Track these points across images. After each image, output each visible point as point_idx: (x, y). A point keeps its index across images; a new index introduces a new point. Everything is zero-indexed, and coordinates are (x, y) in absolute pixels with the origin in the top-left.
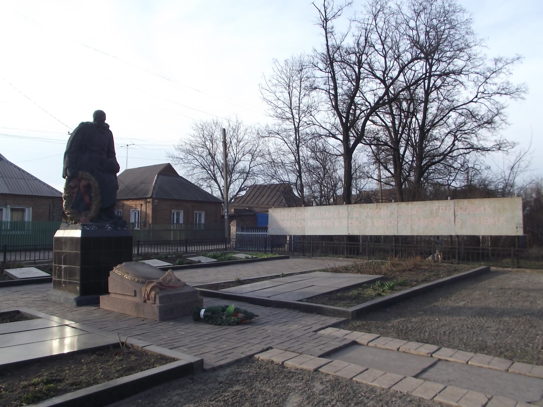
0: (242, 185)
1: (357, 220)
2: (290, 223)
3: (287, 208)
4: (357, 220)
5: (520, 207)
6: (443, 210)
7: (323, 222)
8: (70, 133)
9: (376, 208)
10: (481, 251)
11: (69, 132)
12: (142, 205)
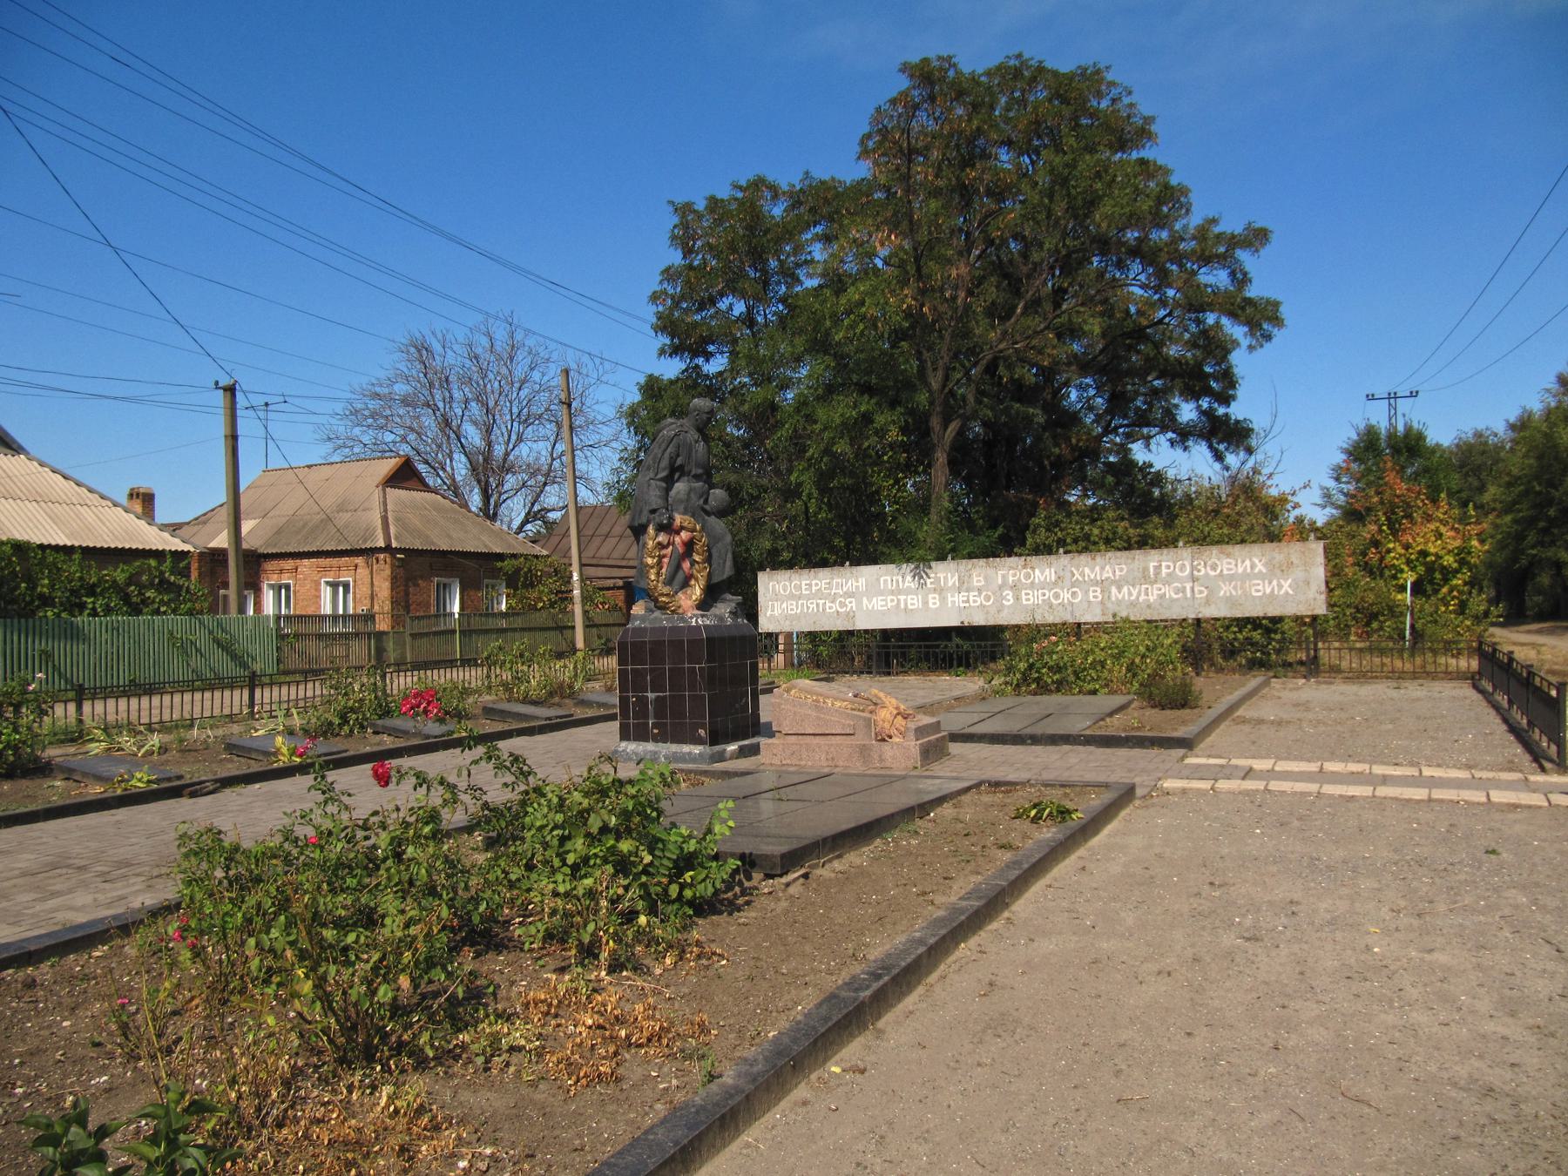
0: (533, 505)
2: (818, 605)
3: (807, 571)
5: (1321, 559)
6: (1168, 567)
7: (899, 600)
9: (1025, 567)
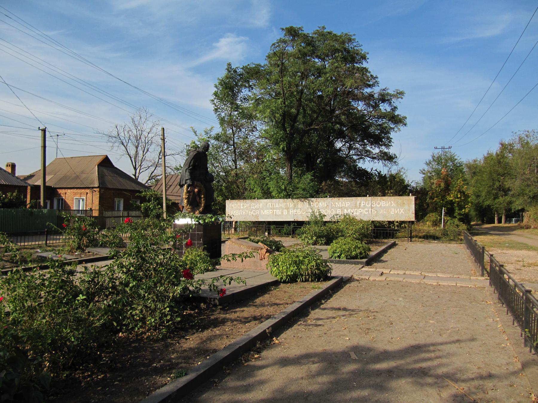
1: (301, 210)
2: (246, 212)
4: (301, 210)
7: (273, 211)
8: (41, 128)
10: (388, 231)
11: (39, 128)
12: (87, 193)
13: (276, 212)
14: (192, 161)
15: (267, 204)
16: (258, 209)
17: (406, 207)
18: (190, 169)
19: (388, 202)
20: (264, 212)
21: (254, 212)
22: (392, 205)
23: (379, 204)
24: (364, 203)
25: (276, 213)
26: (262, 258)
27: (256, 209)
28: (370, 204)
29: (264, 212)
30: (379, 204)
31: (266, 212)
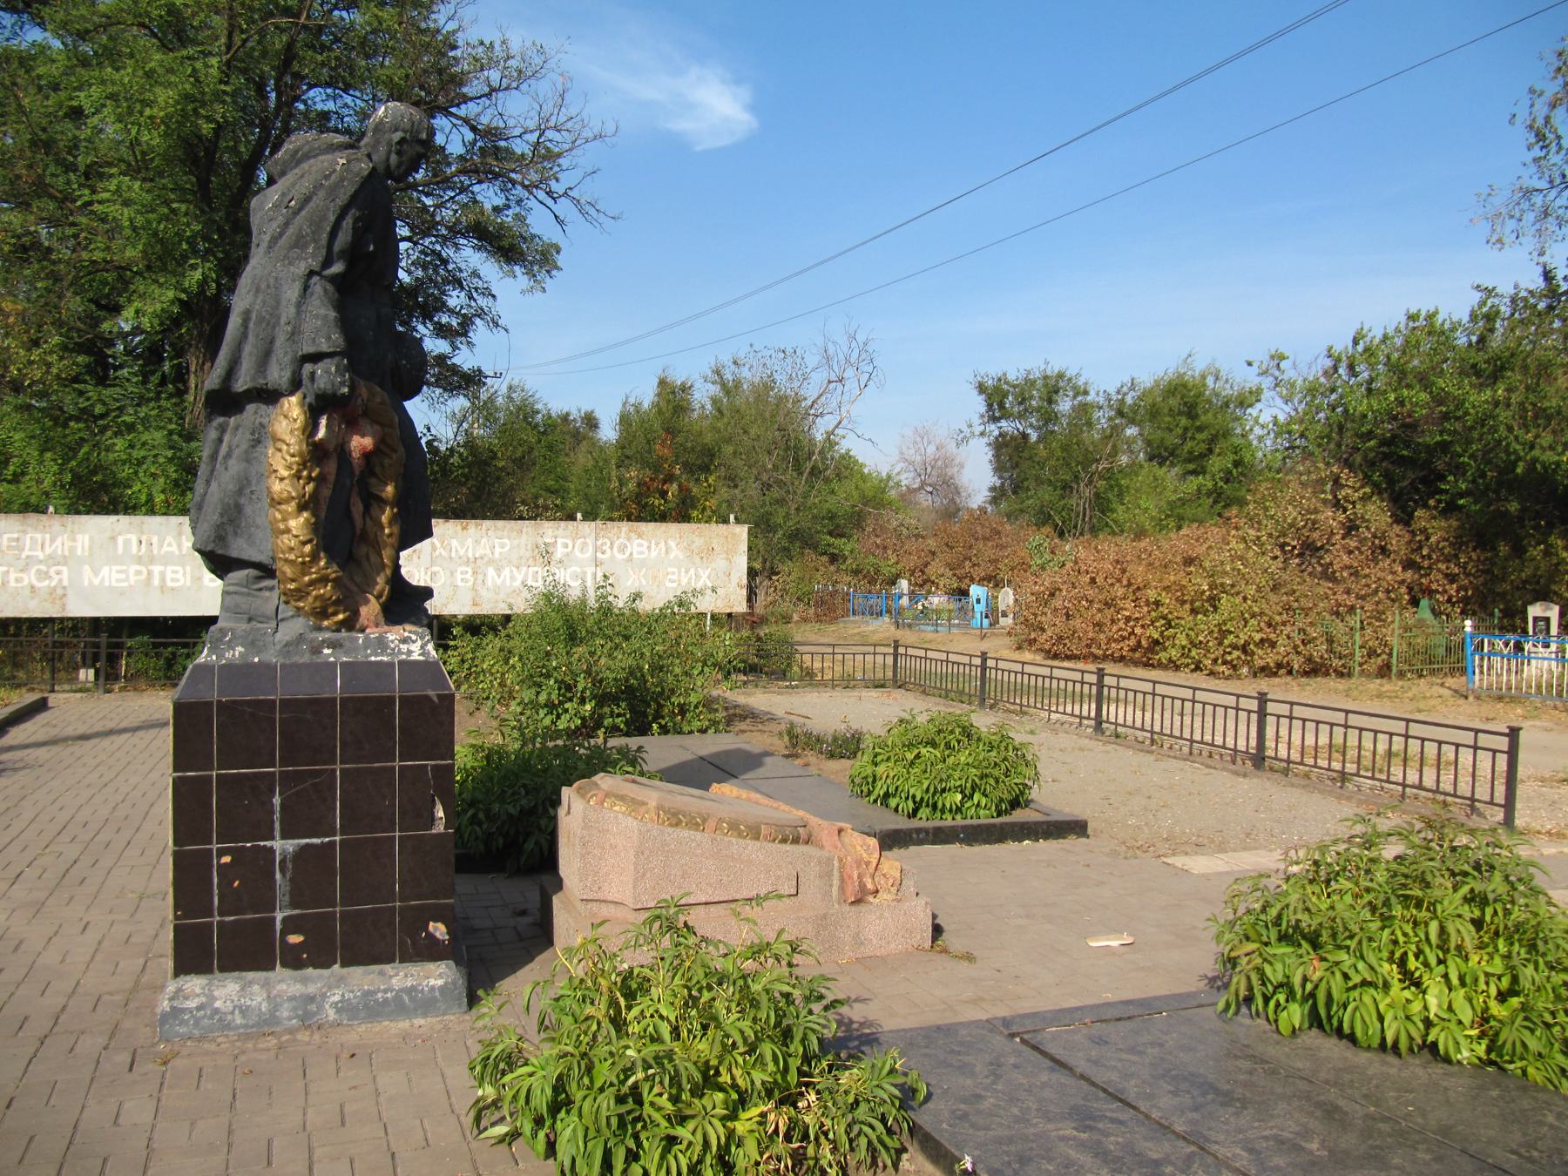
7: (150, 573)
13: (163, 575)
14: (348, 223)
15: (113, 539)
16: (64, 561)
17: (720, 563)
18: (333, 279)
19: (657, 544)
20: (96, 573)
21: (45, 575)
22: (672, 556)
23: (622, 549)
24: (566, 546)
25: (163, 579)
26: (862, 886)
27: (53, 560)
28: (591, 549)
29: (96, 573)
30: (622, 549)
31: (110, 576)
